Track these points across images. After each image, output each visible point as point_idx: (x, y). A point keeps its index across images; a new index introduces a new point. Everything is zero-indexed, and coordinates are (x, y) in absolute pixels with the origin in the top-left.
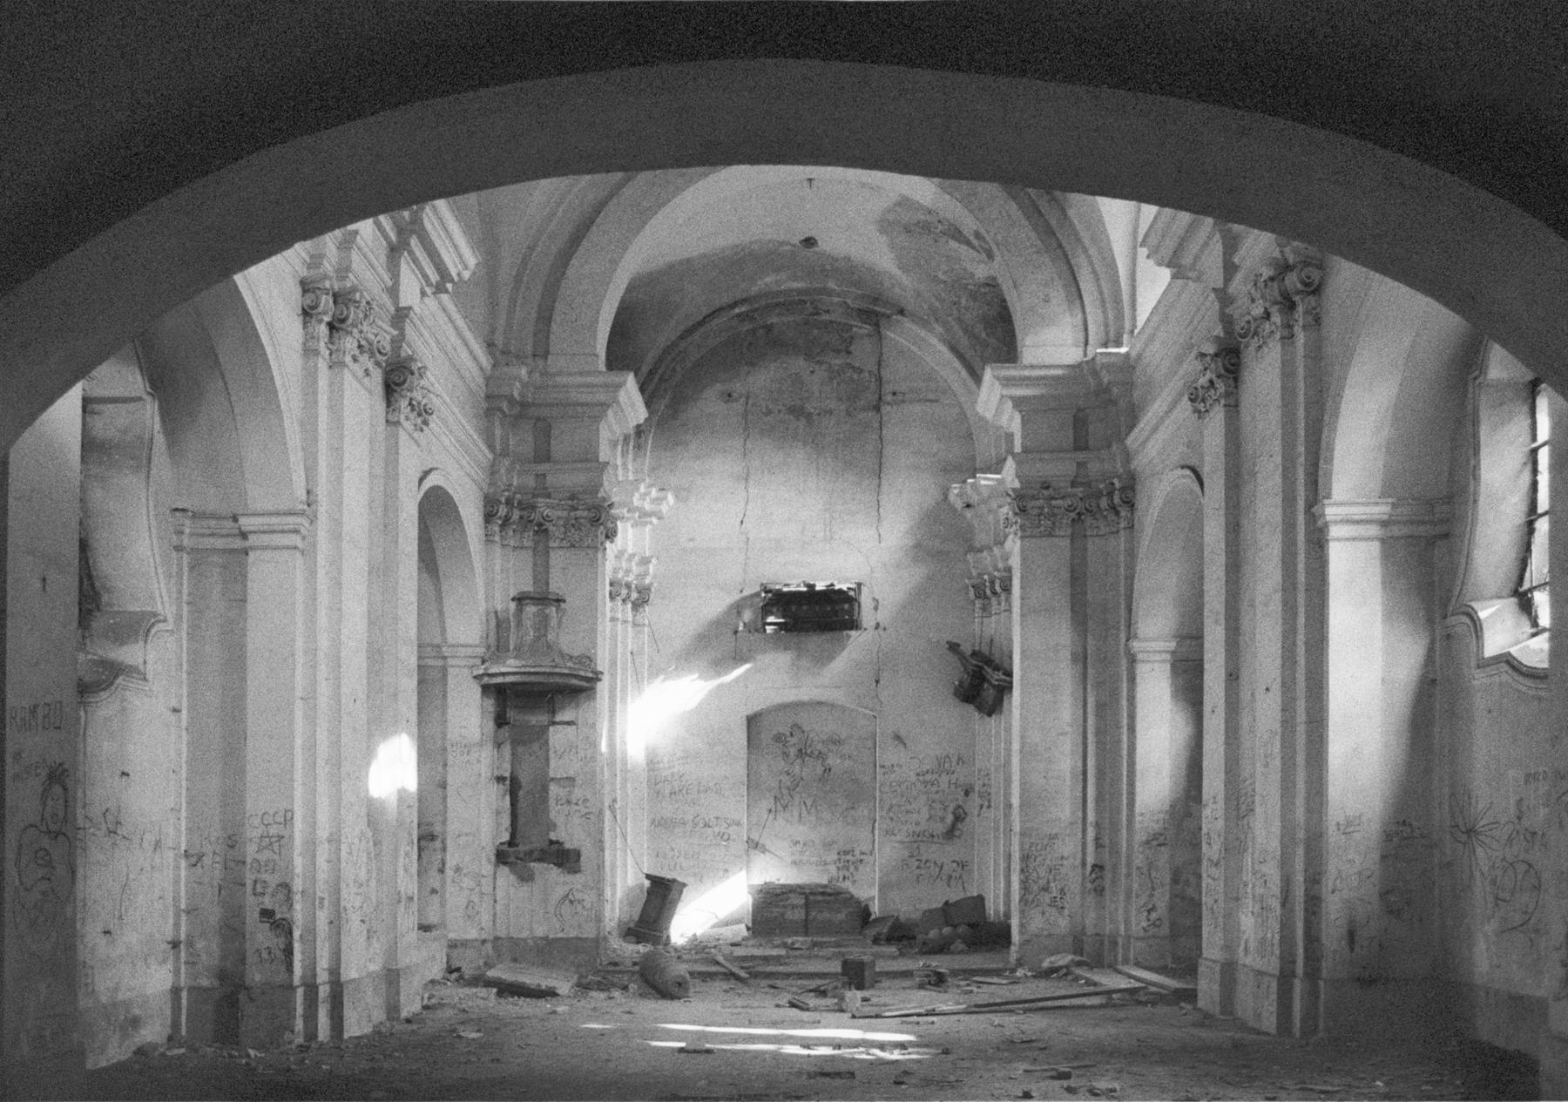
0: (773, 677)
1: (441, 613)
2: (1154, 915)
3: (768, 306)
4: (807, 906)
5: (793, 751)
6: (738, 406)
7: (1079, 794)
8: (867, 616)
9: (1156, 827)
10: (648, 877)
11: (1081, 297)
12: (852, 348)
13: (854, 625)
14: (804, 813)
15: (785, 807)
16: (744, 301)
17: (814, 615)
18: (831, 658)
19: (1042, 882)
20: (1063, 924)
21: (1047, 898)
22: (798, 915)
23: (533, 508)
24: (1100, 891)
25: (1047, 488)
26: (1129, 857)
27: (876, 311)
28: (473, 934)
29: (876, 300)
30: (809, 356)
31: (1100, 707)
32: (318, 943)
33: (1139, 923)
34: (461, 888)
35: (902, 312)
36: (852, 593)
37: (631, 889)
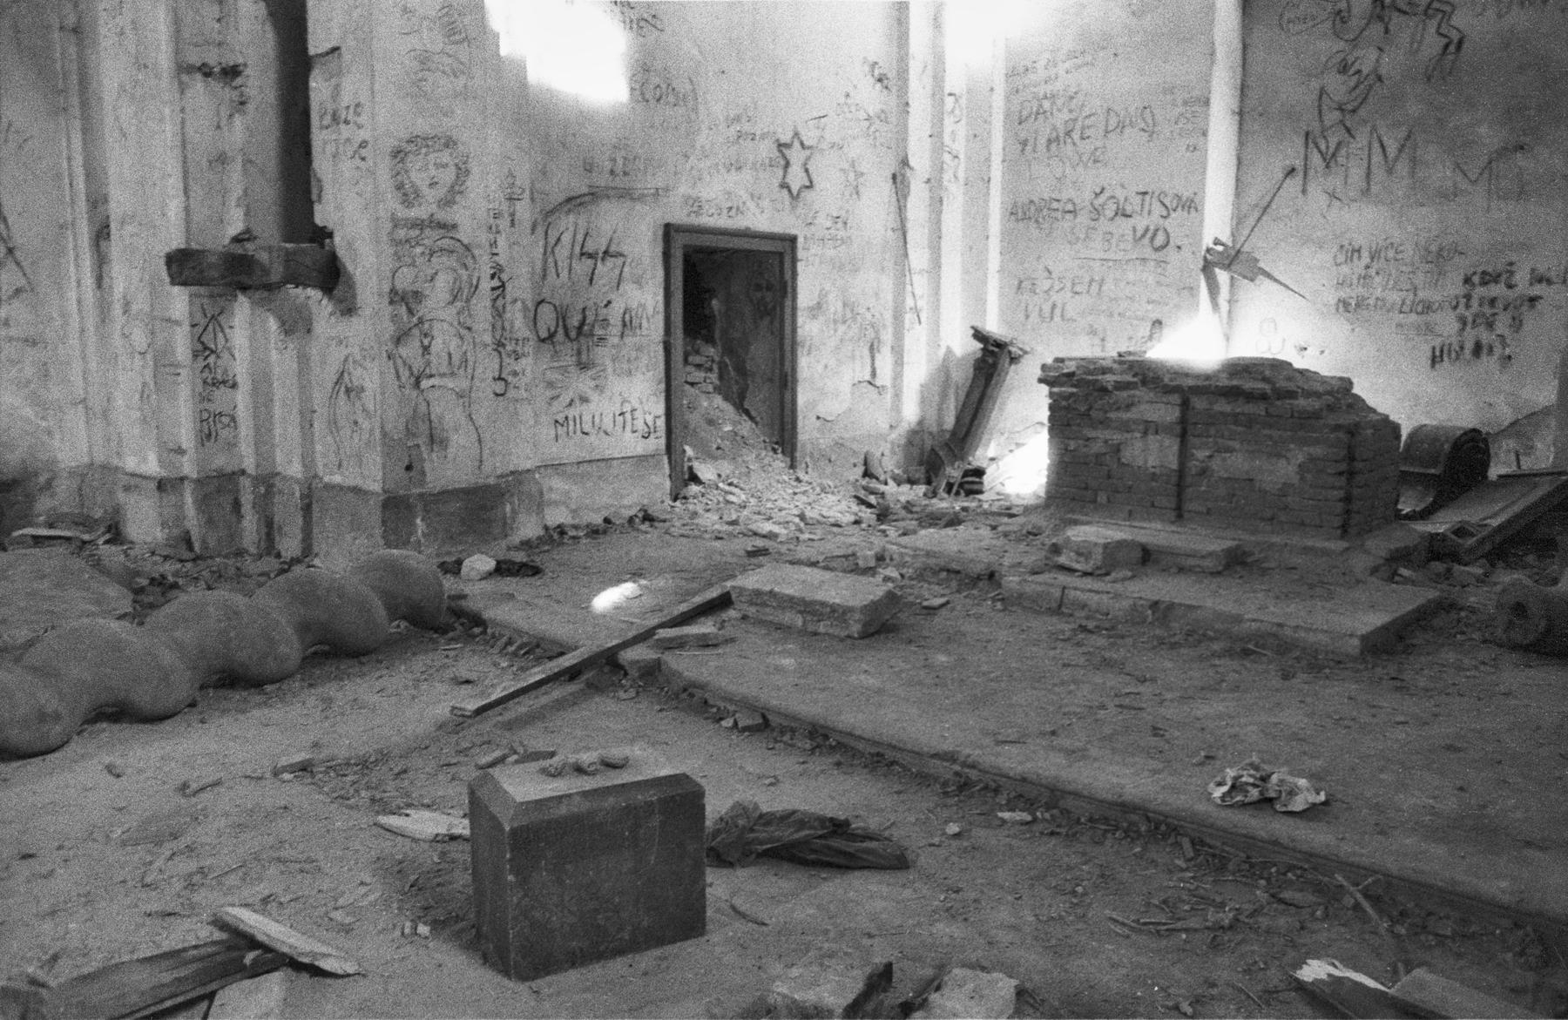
4: (1184, 431)
14: (1379, 174)
15: (1329, 160)
32: (277, 411)
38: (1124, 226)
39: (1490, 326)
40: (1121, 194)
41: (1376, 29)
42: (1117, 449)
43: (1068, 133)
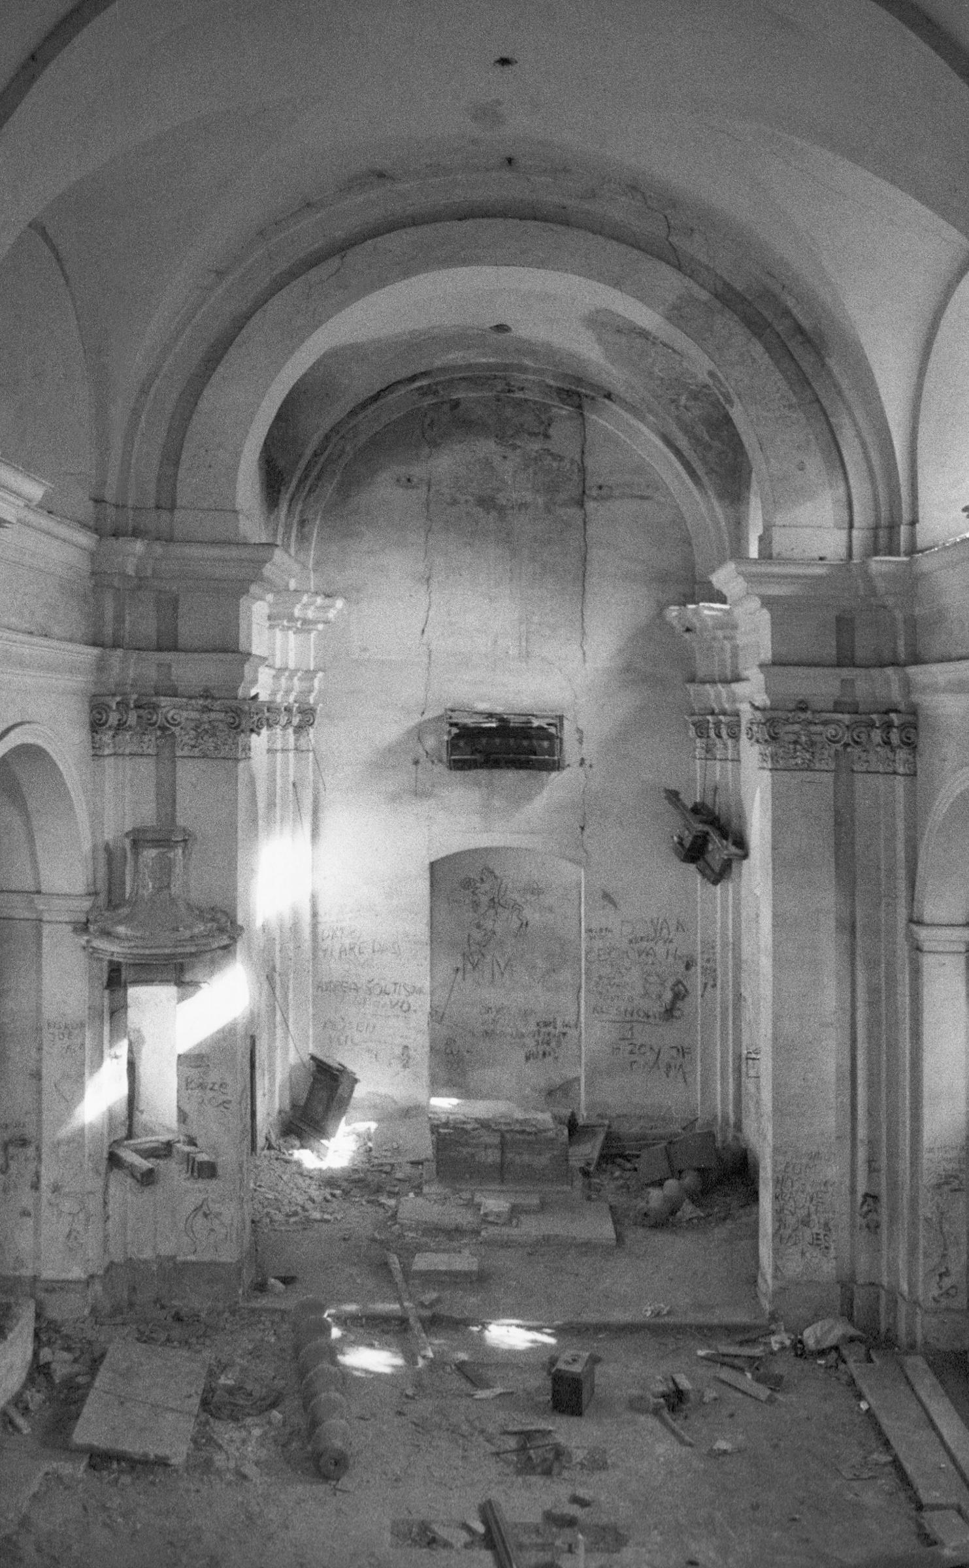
0: (464, 818)
1: (33, 854)
2: (947, 1282)
3: (452, 381)
4: (503, 1146)
5: (484, 900)
7: (847, 1100)
8: (571, 750)
9: (949, 1167)
10: (313, 1058)
11: (845, 473)
12: (551, 431)
13: (556, 766)
16: (424, 374)
17: (498, 747)
18: (529, 798)
19: (802, 1213)
20: (828, 1268)
21: (808, 1233)
22: (492, 1157)
23: (155, 707)
24: (874, 1228)
25: (804, 710)
26: (914, 1201)
27: (578, 393)
28: (77, 1273)
29: (579, 380)
30: (500, 438)
31: (873, 990)
33: (927, 1292)
34: (60, 1213)
35: (608, 396)
36: (552, 730)
37: (293, 1068)
38: (386, 999)
39: (548, 1044)
40: (383, 983)
41: (492, 912)
42: (473, 1156)
43: (351, 949)
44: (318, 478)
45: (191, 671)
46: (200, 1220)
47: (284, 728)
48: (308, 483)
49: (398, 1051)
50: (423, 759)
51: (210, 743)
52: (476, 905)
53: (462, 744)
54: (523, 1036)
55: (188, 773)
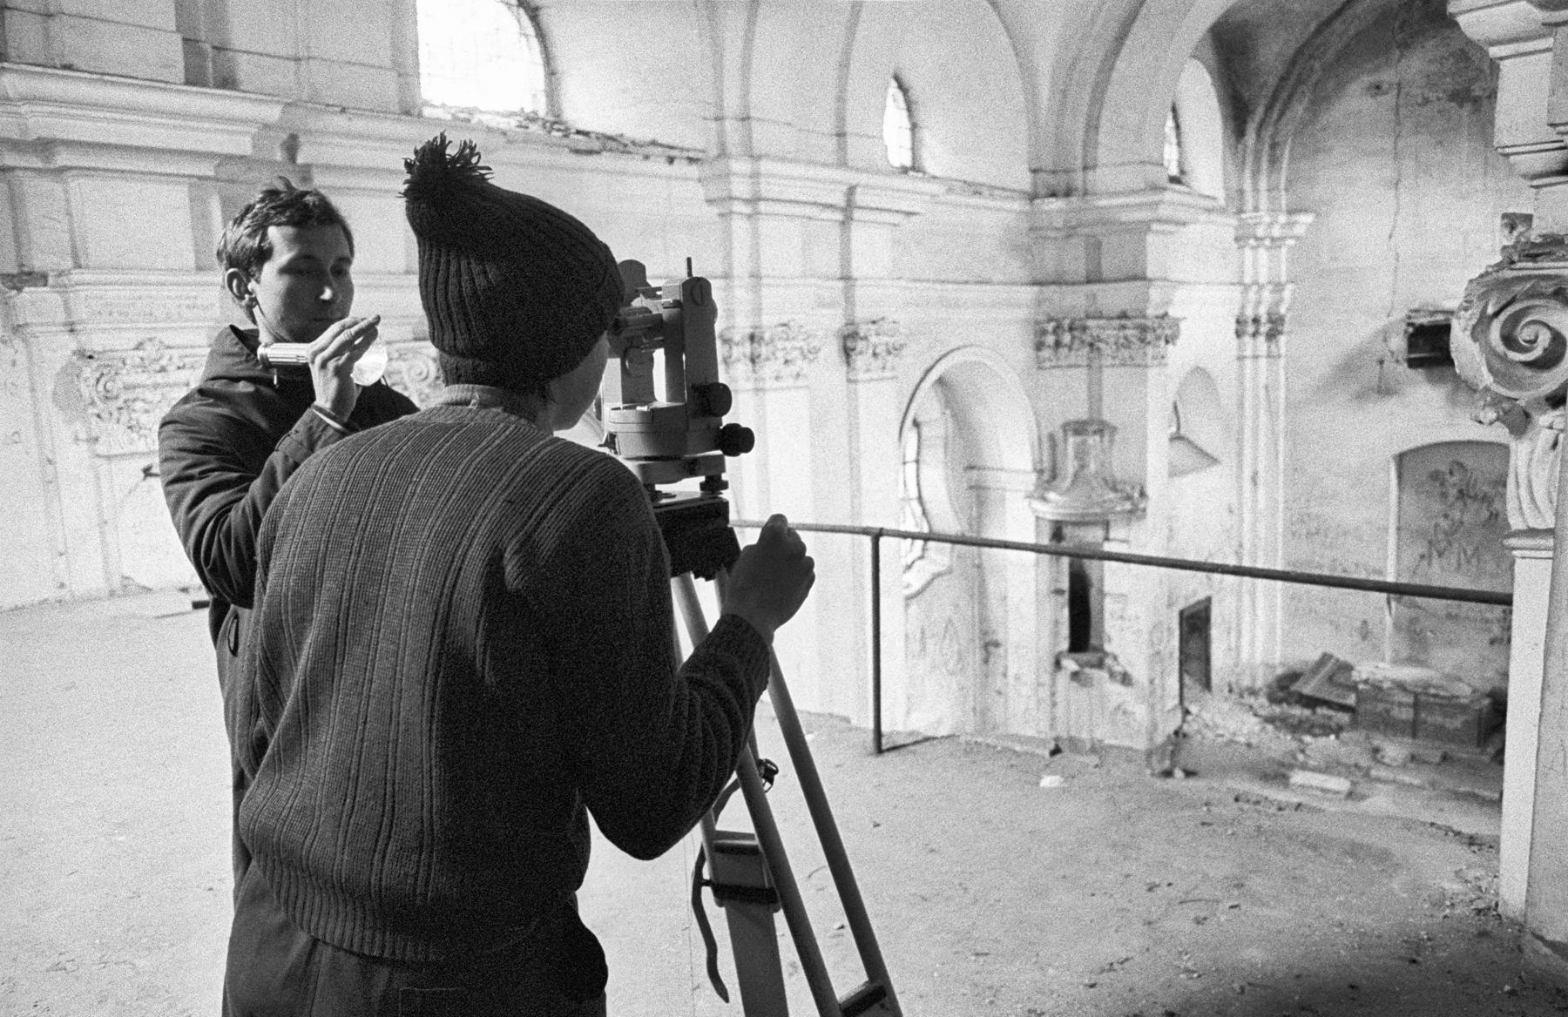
4: (1416, 706)
5: (1453, 492)
6: (1389, 99)
22: (1406, 714)
23: (1084, 329)
44: (1290, 97)
45: (1114, 297)
46: (1119, 716)
47: (1255, 335)
48: (1278, 106)
49: (1358, 624)
50: (1388, 358)
51: (1126, 353)
52: (1444, 495)
53: (1421, 342)
54: (1487, 621)
55: (1111, 377)
